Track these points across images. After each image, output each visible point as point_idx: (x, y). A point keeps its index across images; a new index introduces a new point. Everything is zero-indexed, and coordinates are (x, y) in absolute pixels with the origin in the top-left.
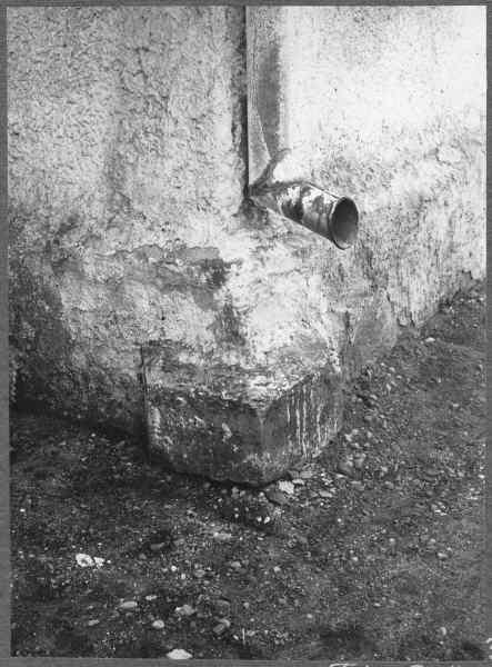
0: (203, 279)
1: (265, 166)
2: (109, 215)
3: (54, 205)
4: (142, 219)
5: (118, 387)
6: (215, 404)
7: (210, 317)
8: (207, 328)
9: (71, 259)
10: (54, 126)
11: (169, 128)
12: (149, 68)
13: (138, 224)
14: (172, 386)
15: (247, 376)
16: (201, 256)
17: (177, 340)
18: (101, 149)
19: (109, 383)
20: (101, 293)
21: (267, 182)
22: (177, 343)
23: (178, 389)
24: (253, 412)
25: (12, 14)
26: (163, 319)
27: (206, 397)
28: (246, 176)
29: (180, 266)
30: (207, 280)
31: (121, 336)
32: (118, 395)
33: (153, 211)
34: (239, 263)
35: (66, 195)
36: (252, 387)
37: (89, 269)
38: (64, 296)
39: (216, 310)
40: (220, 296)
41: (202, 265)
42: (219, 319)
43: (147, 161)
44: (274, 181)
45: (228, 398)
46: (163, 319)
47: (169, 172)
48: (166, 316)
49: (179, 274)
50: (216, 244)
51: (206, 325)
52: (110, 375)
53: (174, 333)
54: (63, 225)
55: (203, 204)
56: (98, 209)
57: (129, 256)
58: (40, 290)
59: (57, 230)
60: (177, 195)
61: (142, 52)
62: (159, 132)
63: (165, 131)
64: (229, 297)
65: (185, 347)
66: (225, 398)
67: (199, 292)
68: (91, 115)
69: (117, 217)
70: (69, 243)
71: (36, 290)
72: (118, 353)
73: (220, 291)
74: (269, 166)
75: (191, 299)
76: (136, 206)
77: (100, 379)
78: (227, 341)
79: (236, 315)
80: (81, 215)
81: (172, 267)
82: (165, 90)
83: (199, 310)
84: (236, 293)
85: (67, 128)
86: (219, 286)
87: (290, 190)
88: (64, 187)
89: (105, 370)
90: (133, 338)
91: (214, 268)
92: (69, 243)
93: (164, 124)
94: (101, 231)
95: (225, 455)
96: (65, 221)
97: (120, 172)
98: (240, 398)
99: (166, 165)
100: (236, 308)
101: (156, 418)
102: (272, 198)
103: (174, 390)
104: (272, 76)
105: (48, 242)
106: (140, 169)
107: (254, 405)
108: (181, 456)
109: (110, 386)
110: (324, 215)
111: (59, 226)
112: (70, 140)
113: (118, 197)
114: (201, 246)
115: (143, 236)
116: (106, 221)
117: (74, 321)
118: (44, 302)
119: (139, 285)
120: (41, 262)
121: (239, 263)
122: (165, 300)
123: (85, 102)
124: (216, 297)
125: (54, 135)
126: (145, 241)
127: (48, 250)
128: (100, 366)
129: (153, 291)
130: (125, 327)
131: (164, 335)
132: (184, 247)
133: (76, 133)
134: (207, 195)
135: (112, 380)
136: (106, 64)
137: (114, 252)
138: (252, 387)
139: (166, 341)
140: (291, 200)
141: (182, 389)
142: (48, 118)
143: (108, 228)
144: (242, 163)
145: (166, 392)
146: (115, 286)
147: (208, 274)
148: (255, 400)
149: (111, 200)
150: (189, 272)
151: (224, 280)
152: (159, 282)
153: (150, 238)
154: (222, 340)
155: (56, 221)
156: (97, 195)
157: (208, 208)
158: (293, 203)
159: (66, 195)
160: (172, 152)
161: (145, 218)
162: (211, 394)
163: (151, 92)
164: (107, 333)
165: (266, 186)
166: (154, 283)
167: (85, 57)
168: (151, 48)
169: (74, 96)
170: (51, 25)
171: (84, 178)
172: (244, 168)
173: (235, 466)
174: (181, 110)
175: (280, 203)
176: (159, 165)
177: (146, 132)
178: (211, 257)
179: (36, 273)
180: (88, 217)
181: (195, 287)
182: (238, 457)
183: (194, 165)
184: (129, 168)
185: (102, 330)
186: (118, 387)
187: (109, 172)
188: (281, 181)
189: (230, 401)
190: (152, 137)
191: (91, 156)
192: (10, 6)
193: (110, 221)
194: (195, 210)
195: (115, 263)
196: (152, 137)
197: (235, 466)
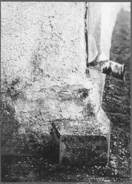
0: (79, 96)
1: (96, 56)
2: (33, 76)
3: (7, 75)
4: (48, 77)
5: (40, 138)
6: (90, 138)
7: (81, 108)
8: (80, 113)
9: (20, 94)
10: (9, 45)
11: (61, 44)
12: (54, 24)
13: (46, 79)
14: (71, 134)
15: (98, 127)
16: (77, 88)
17: (68, 118)
18: (30, 53)
19: (37, 137)
20: (34, 105)
21: (97, 61)
22: (68, 119)
23: (74, 135)
24: (105, 139)
25: (1, 2)
26: (61, 111)
27: (86, 136)
28: (87, 60)
29: (69, 92)
30: (81, 96)
31: (43, 119)
32: (40, 141)
33: (53, 74)
34: (92, 89)
35: (13, 70)
36: (102, 130)
37: (29, 97)
38: (16, 108)
39: (84, 106)
40: (86, 101)
41: (78, 91)
42: (85, 109)
43: (52, 56)
44: (99, 61)
45: (95, 135)
46: (61, 111)
47: (61, 60)
48: (62, 110)
49: (69, 95)
50: (81, 83)
51: (79, 111)
52: (37, 135)
53: (66, 116)
54: (13, 82)
55: (74, 70)
56: (28, 74)
57: (46, 90)
58: (5, 107)
59: (11, 84)
60: (63, 67)
61: (51, 18)
62: (57, 46)
63: (59, 45)
64: (90, 101)
65: (71, 120)
66: (93, 135)
67: (77, 100)
68: (26, 41)
69: (37, 77)
70: (18, 88)
71: (3, 107)
72: (41, 126)
73: (86, 99)
74: (97, 56)
75: (74, 103)
76: (46, 73)
77: (32, 137)
78: (88, 116)
79: (92, 107)
80: (21, 77)
81: (65, 93)
82: (60, 31)
83: (77, 107)
84: (92, 99)
85: (15, 46)
86: (85, 97)
87: (106, 63)
88: (12, 68)
89: (34, 133)
90: (49, 120)
91: (83, 91)
92: (18, 88)
93: (59, 43)
94: (31, 83)
95: (93, 155)
96: (14, 80)
97: (39, 61)
98: (99, 134)
99: (60, 57)
100: (92, 104)
101: (63, 146)
102: (99, 66)
103: (72, 135)
104: (100, 26)
105: (8, 89)
106: (48, 59)
107: (105, 136)
108: (74, 159)
109: (36, 139)
110: (120, 71)
111: (12, 82)
112: (16, 50)
113: (37, 70)
114: (76, 84)
115: (49, 83)
116: (33, 79)
117: (20, 116)
118: (7, 111)
119: (51, 100)
120: (6, 96)
121: (92, 89)
122: (62, 105)
123: (24, 36)
124: (84, 101)
125: (9, 49)
126: (52, 85)
127: (9, 91)
128: (32, 132)
129: (57, 102)
130: (45, 116)
131: (62, 117)
132: (68, 86)
133: (19, 48)
134: (76, 67)
135: (38, 136)
136: (34, 22)
137: (40, 90)
138: (102, 130)
139: (63, 119)
140: (107, 67)
141: (75, 135)
142: (6, 42)
143: (34, 81)
144: (87, 55)
145: (68, 136)
146: (40, 102)
147: (81, 94)
148: (105, 134)
149: (34, 71)
150: (73, 94)
151: (88, 95)
152: (60, 99)
153: (53, 83)
154: (86, 116)
155: (10, 81)
156: (27, 70)
157: (76, 71)
158: (108, 68)
159: (13, 70)
160: (62, 53)
161: (49, 76)
162: (87, 134)
163: (54, 31)
164: (36, 119)
165: (97, 62)
166: (57, 99)
167: (25, 20)
168: (55, 16)
169: (18, 34)
170: (10, 8)
171: (22, 64)
172: (87, 57)
173: (96, 158)
174: (67, 38)
175: (102, 68)
176: (57, 57)
177: (52, 46)
178: (81, 88)
179: (3, 101)
180: (24, 78)
181: (75, 98)
182: (97, 155)
183: (71, 56)
184: (43, 59)
185: (34, 118)
186: (40, 138)
187: (33, 61)
188: (102, 60)
189: (96, 136)
190: (54, 48)
191: (25, 56)
192: (2, 1)
193: (34, 78)
194: (71, 72)
195: (41, 93)
196: (54, 48)
197: (96, 158)
